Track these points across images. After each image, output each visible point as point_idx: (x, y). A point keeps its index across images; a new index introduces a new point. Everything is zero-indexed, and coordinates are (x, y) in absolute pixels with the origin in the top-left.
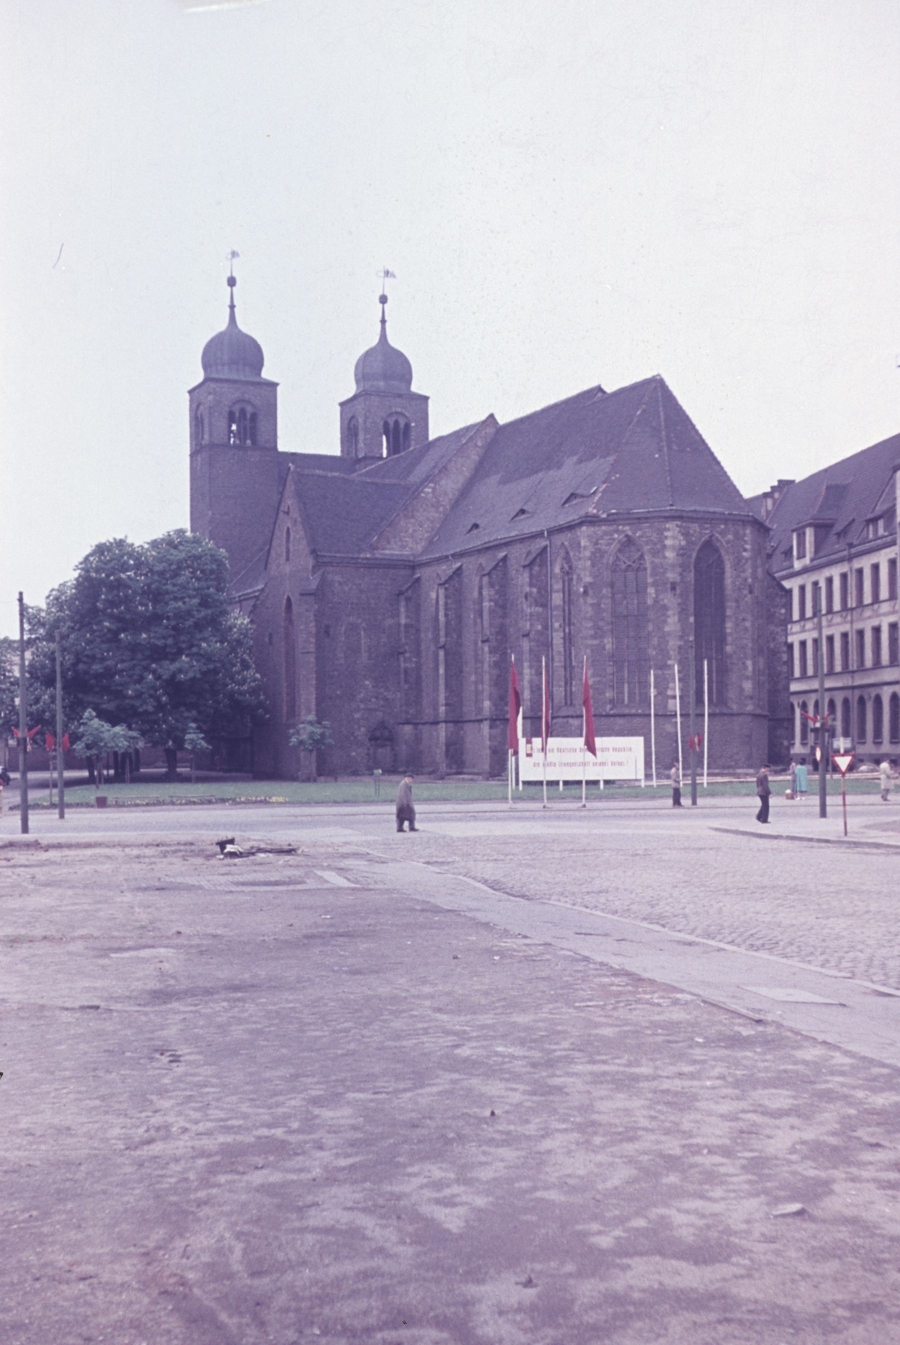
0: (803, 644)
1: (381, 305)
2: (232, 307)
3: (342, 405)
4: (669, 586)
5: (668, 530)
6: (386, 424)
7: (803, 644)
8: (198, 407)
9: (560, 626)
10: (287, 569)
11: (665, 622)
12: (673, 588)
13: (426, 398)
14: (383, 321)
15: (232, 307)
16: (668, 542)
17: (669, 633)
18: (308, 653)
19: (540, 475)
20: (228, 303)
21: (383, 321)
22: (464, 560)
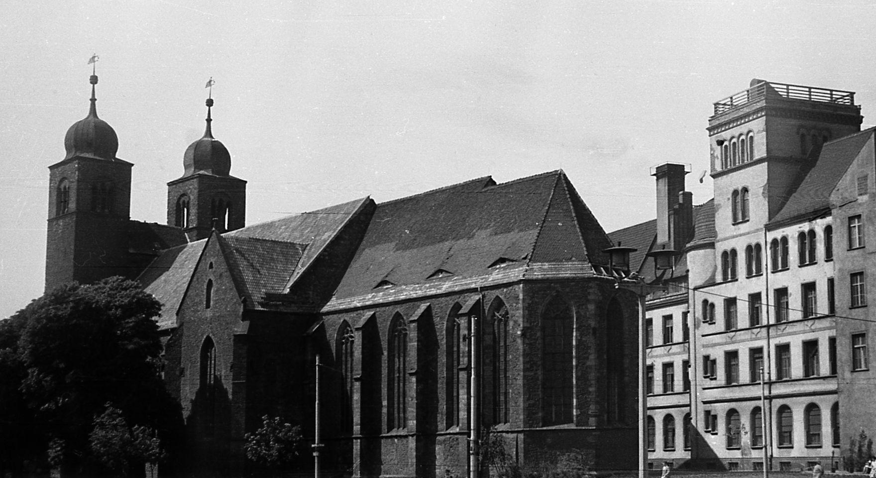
0: (668, 366)
1: (208, 108)
2: (93, 100)
3: (169, 184)
4: (591, 331)
5: (591, 288)
6: (213, 202)
7: (668, 366)
8: (61, 181)
9: (491, 361)
10: (209, 313)
11: (588, 358)
12: (594, 333)
13: (684, 166)
14: (209, 120)
15: (93, 100)
16: (591, 297)
17: (590, 367)
18: (517, 438)
19: (447, 244)
20: (90, 97)
21: (209, 120)
22: (378, 309)
